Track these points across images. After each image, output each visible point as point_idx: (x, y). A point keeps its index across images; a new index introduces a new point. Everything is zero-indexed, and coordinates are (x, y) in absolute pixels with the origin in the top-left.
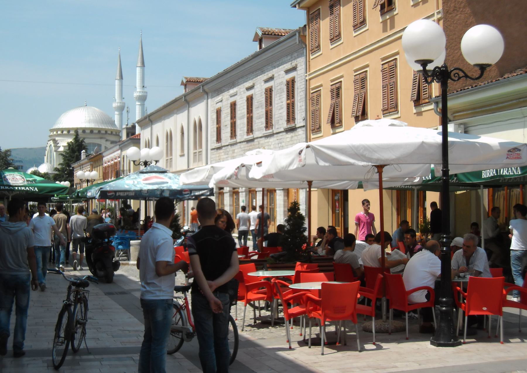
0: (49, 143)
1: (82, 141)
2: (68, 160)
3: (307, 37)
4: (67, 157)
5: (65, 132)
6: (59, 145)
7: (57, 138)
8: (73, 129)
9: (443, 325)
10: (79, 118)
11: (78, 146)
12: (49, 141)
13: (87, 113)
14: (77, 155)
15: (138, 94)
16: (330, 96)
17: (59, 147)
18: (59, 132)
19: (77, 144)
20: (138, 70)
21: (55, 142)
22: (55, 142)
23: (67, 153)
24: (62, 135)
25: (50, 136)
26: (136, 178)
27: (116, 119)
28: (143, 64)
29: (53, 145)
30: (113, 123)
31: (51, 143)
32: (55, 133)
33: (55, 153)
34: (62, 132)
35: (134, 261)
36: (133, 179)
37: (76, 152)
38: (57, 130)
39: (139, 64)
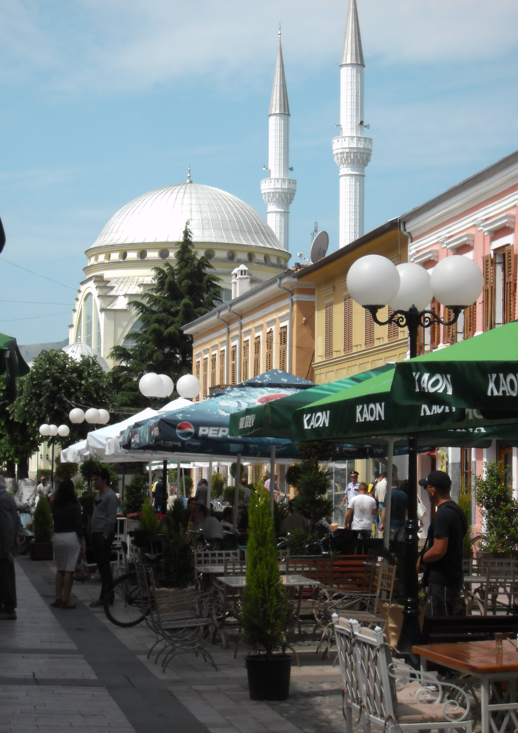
0: (83, 288)
1: (204, 263)
2: (159, 321)
3: (294, 344)
4: (153, 312)
5: (132, 255)
6: (113, 293)
7: (107, 274)
8: (153, 246)
9: (393, 530)
10: (166, 217)
11: (188, 276)
12: (82, 283)
13: (194, 201)
14: (186, 305)
15: (346, 144)
16: (369, 380)
17: (116, 297)
18: (115, 256)
19: (187, 270)
20: (274, 125)
21: (103, 283)
22: (103, 283)
23: (155, 301)
24: (124, 262)
25: (87, 269)
26: (242, 396)
27: (273, 222)
28: (285, 112)
29: (95, 293)
30: (267, 233)
31: (91, 287)
32: (102, 258)
33: (102, 316)
34: (124, 256)
35: (480, 331)
36: (235, 397)
37: (182, 297)
38: (108, 250)
39: (276, 107)
